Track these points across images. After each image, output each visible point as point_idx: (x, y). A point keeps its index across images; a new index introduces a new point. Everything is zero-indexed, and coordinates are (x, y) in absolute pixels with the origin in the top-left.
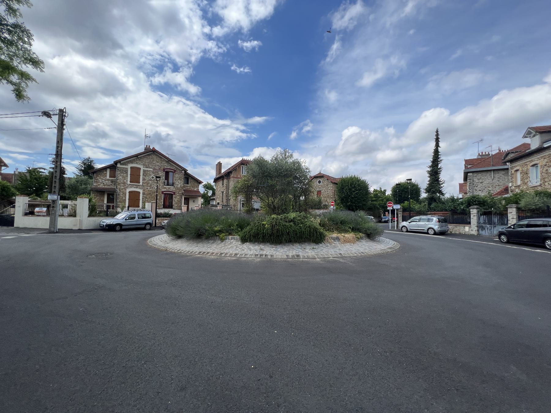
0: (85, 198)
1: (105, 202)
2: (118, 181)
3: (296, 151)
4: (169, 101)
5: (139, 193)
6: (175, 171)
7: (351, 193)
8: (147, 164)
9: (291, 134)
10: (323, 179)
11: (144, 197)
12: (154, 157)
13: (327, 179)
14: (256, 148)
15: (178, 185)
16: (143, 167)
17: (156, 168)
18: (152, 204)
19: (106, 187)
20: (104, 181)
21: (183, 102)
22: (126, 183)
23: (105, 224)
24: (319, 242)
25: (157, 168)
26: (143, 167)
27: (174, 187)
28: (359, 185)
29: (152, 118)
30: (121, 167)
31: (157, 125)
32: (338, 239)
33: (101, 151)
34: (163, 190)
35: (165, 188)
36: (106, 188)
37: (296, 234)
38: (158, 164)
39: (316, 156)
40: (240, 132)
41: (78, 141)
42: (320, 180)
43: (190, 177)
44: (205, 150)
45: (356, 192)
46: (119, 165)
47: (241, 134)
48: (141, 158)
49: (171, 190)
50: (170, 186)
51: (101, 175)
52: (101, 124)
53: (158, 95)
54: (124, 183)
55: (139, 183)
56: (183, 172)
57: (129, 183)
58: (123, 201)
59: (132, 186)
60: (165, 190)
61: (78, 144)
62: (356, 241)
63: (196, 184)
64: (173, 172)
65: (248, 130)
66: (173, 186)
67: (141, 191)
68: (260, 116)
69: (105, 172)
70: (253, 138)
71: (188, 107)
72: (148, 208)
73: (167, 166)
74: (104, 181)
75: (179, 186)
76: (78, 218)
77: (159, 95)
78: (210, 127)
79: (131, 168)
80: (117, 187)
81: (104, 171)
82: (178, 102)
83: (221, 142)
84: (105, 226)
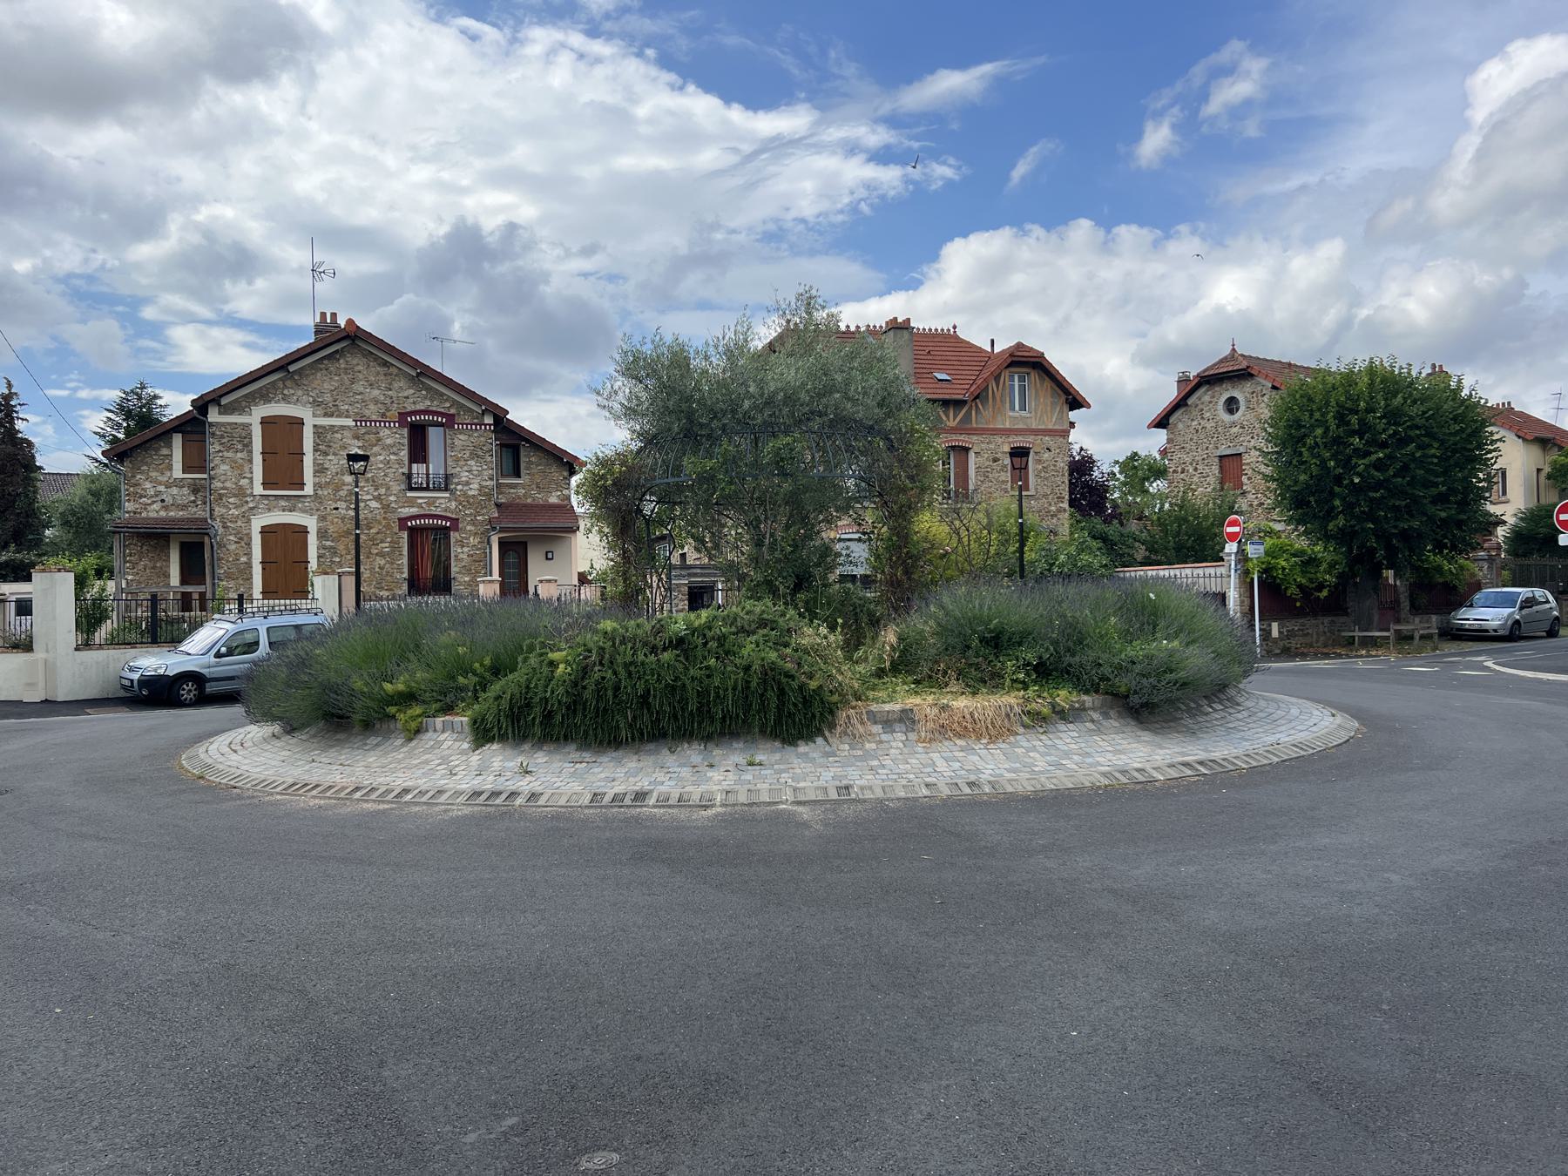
0: (59, 570)
1: (175, 580)
2: (217, 484)
3: (1183, 228)
4: (507, 54)
5: (303, 531)
6: (451, 418)
7: (1347, 464)
8: (328, 398)
9: (1138, 136)
10: (1248, 386)
11: (325, 548)
12: (355, 362)
13: (1274, 388)
14: (949, 244)
15: (468, 484)
16: (314, 415)
17: (367, 413)
18: (343, 578)
19: (172, 514)
20: (162, 488)
21: (572, 50)
22: (248, 492)
23: (136, 676)
24: (801, 737)
25: (372, 411)
26: (314, 415)
27: (452, 492)
28: (1393, 416)
29: (436, 156)
30: (223, 424)
31: (465, 182)
32: (907, 719)
33: (240, 336)
34: (407, 511)
35: (411, 502)
36: (173, 520)
37: (684, 701)
38: (376, 392)
39: (1309, 242)
40: (870, 160)
41: (147, 301)
42: (1236, 394)
43: (527, 441)
44: (692, 283)
45: (1374, 457)
46: (214, 416)
47: (872, 172)
48: (300, 372)
49: (438, 512)
50: (434, 490)
51: (148, 465)
52: (228, 212)
53: (457, 32)
54: (241, 493)
55: (301, 485)
56: (489, 420)
57: (258, 489)
58: (241, 572)
59: (270, 503)
60: (414, 511)
61: (149, 313)
62: (1021, 730)
63: (556, 474)
64: (441, 425)
65: (907, 143)
66: (446, 489)
67: (311, 523)
68: (961, 64)
69: (165, 451)
70: (940, 183)
71: (600, 71)
72: (324, 598)
73: (415, 400)
74: (162, 488)
75: (475, 486)
76: (39, 654)
77: (464, 31)
78: (708, 158)
79: (265, 422)
80: (212, 510)
81: (157, 450)
82: (551, 53)
83: (772, 227)
84: (135, 683)
